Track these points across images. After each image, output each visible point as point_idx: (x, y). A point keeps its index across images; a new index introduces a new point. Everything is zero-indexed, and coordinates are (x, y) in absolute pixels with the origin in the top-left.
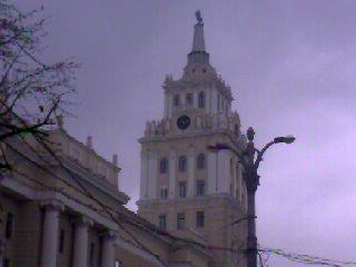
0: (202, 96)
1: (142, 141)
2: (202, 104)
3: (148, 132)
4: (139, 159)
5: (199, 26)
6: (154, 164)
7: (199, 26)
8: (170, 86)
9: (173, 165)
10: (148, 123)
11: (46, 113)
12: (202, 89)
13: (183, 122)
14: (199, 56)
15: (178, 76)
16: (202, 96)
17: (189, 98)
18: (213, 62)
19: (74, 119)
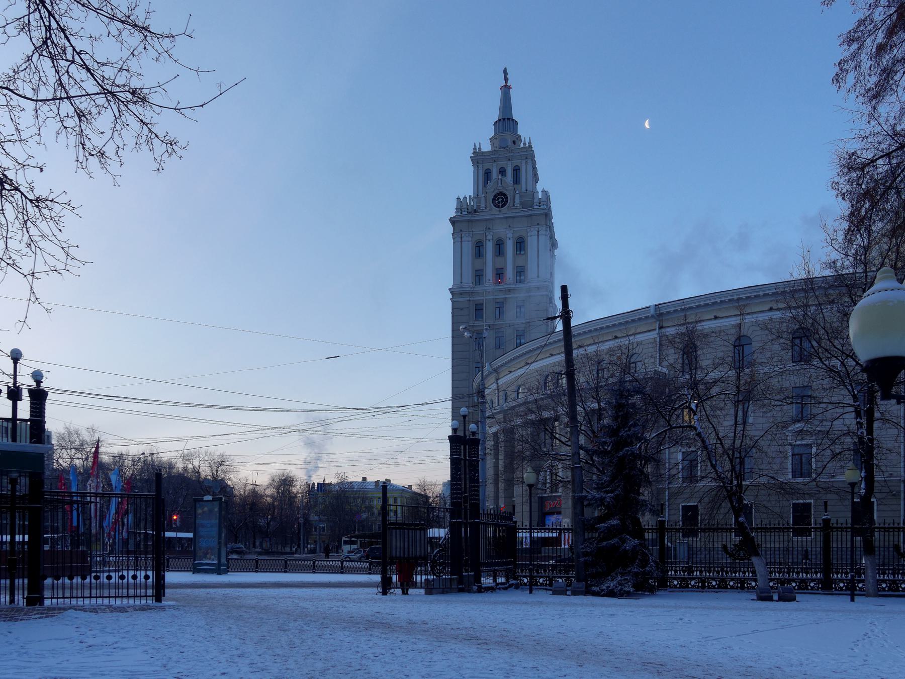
0: (517, 170)
1: (453, 221)
2: (517, 180)
3: (460, 209)
4: (451, 241)
5: (506, 89)
6: (468, 247)
7: (506, 89)
8: (478, 158)
9: (489, 248)
10: (458, 199)
11: (708, 408)
12: (516, 162)
13: (500, 200)
14: (506, 123)
15: (487, 147)
16: (517, 170)
17: (502, 172)
18: (522, 131)
19: (101, 450)
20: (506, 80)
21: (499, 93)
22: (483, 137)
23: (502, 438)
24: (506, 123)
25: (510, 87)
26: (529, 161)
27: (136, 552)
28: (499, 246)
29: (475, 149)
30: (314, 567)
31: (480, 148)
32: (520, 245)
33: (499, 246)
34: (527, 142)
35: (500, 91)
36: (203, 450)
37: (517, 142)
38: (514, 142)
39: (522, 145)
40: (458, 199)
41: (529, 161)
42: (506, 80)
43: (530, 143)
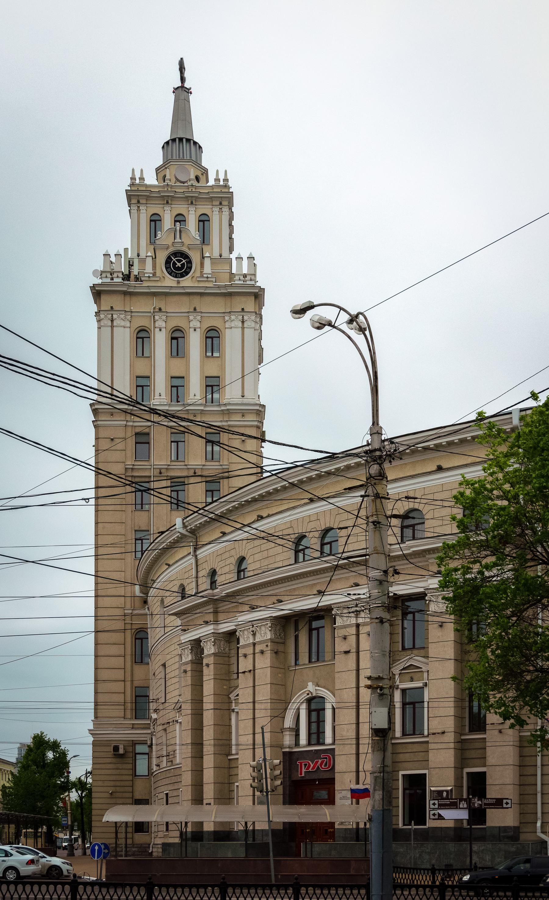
0: (204, 221)
5: (182, 92)
6: (124, 337)
7: (182, 92)
13: (179, 264)
14: (182, 145)
20: (183, 79)
21: (169, 101)
22: (147, 162)
23: (209, 649)
24: (182, 145)
25: (188, 91)
26: (226, 209)
27: (520, 741)
28: (177, 337)
29: (133, 179)
30: (169, 565)
31: (142, 179)
32: (212, 338)
33: (177, 337)
34: (222, 177)
35: (173, 96)
36: (62, 747)
37: (203, 179)
38: (197, 179)
39: (211, 182)
40: (107, 255)
41: (226, 209)
42: (183, 79)
43: (226, 180)
